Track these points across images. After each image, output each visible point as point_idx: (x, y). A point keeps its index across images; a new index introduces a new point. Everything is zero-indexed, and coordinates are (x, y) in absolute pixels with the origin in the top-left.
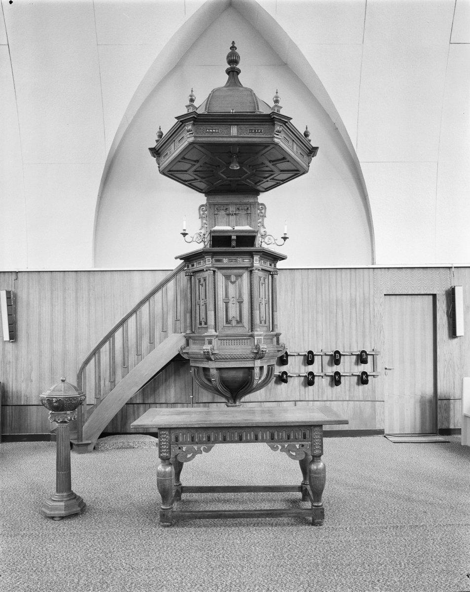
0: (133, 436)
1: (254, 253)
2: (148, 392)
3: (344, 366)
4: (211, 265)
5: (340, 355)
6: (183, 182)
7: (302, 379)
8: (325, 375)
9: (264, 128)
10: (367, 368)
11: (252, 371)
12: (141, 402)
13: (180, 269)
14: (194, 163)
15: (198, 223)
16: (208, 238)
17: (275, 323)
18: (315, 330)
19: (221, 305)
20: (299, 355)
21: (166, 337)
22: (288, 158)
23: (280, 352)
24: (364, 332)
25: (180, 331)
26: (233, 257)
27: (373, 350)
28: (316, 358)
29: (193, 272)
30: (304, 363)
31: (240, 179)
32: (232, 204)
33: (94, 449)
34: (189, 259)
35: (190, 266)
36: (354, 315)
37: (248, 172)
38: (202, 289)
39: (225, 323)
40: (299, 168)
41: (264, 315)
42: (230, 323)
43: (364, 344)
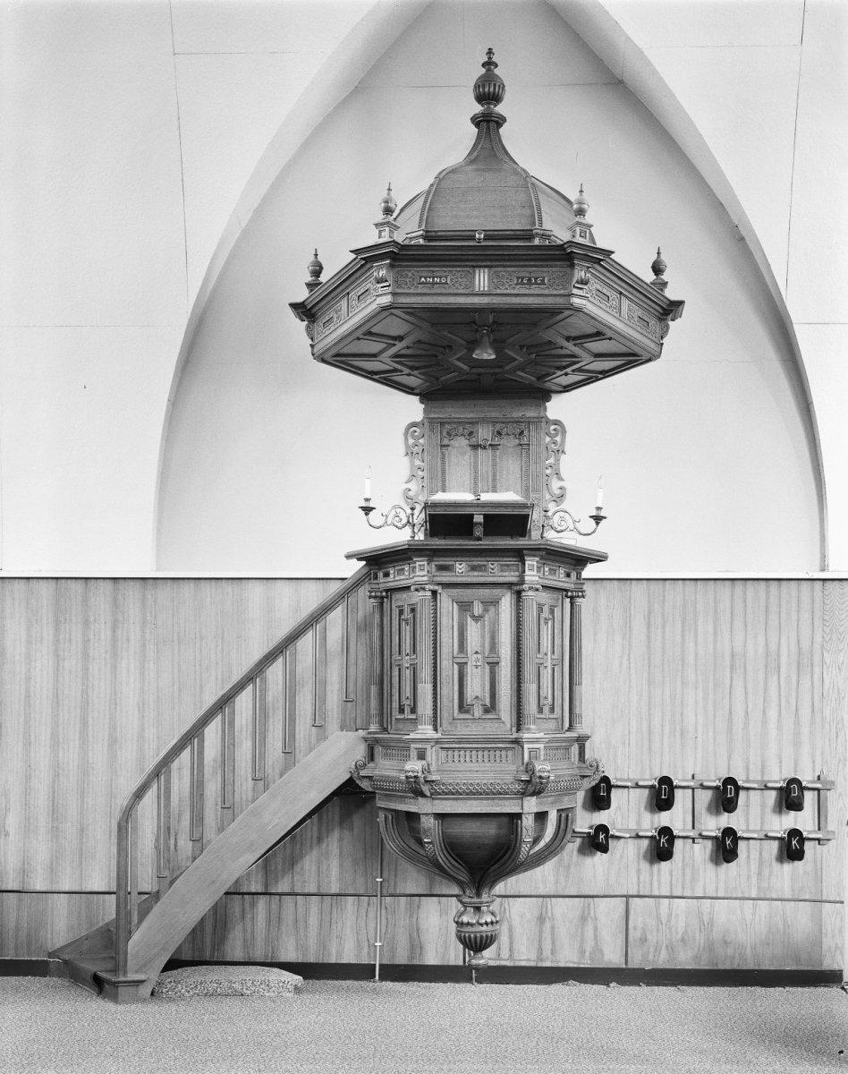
0: (241, 968)
1: (525, 552)
2: (276, 867)
3: (747, 814)
4: (425, 578)
5: (738, 788)
6: (370, 375)
7: (646, 843)
8: (700, 835)
9: (548, 273)
10: (804, 820)
12: (260, 889)
13: (357, 583)
14: (392, 342)
15: (403, 466)
16: (419, 517)
17: (577, 711)
18: (678, 728)
19: (448, 670)
20: (637, 786)
21: (322, 737)
22: (609, 333)
23: (586, 779)
24: (797, 734)
25: (352, 725)
26: (477, 562)
27: (819, 778)
28: (678, 794)
29: (387, 591)
30: (651, 806)
31: (500, 370)
32: (484, 420)
33: (152, 994)
34: (377, 561)
35: (381, 574)
36: (773, 692)
37: (518, 358)
38: (407, 630)
39: (456, 710)
40: (637, 350)
41: (550, 692)
42: (467, 712)
43: (796, 764)
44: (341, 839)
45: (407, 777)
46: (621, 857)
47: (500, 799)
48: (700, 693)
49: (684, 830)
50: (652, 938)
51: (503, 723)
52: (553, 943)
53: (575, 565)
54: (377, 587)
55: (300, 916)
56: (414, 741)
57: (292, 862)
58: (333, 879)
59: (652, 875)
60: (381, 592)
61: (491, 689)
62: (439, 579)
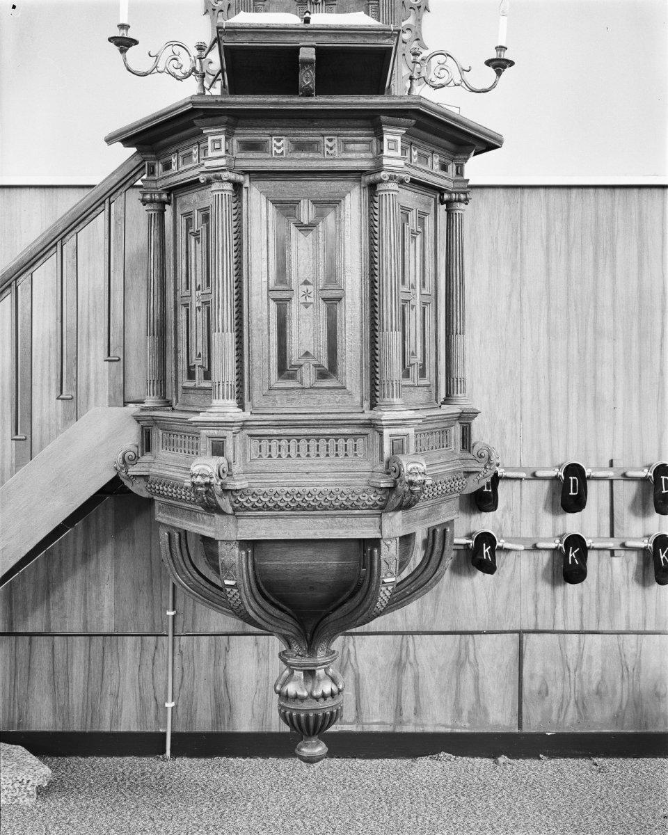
1: (383, 118)
2: (25, 597)
4: (222, 162)
7: (545, 557)
8: (623, 545)
11: (372, 552)
13: (124, 182)
17: (458, 373)
19: (261, 310)
20: (534, 477)
23: (472, 477)
26: (306, 135)
28: (592, 486)
30: (553, 503)
35: (159, 167)
38: (197, 250)
41: (419, 345)
44: (116, 555)
45: (193, 484)
46: (512, 578)
47: (344, 516)
48: (620, 344)
49: (599, 537)
50: (555, 691)
51: (350, 394)
52: (417, 698)
53: (455, 153)
54: (154, 185)
55: (59, 667)
56: (206, 424)
57: (48, 588)
58: (106, 611)
59: (554, 601)
60: (160, 194)
61: (329, 341)
62: (244, 164)
